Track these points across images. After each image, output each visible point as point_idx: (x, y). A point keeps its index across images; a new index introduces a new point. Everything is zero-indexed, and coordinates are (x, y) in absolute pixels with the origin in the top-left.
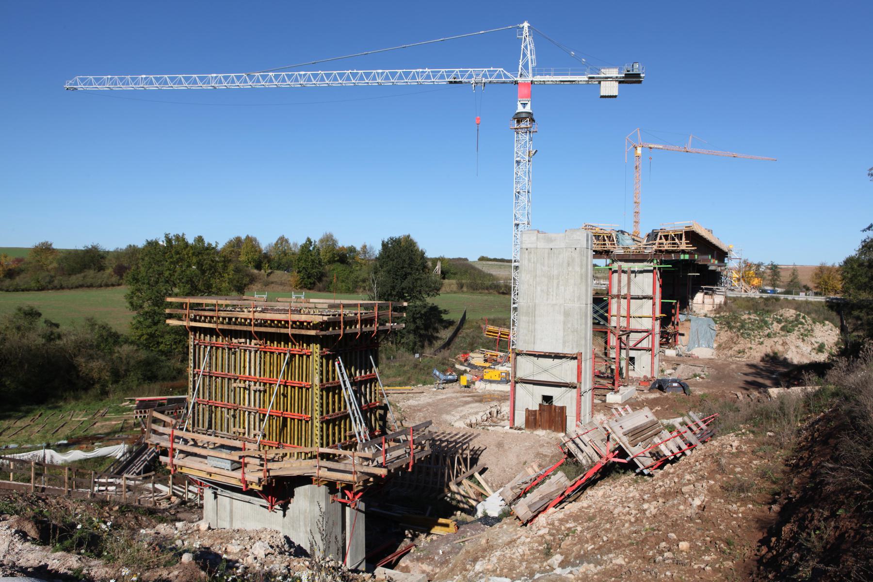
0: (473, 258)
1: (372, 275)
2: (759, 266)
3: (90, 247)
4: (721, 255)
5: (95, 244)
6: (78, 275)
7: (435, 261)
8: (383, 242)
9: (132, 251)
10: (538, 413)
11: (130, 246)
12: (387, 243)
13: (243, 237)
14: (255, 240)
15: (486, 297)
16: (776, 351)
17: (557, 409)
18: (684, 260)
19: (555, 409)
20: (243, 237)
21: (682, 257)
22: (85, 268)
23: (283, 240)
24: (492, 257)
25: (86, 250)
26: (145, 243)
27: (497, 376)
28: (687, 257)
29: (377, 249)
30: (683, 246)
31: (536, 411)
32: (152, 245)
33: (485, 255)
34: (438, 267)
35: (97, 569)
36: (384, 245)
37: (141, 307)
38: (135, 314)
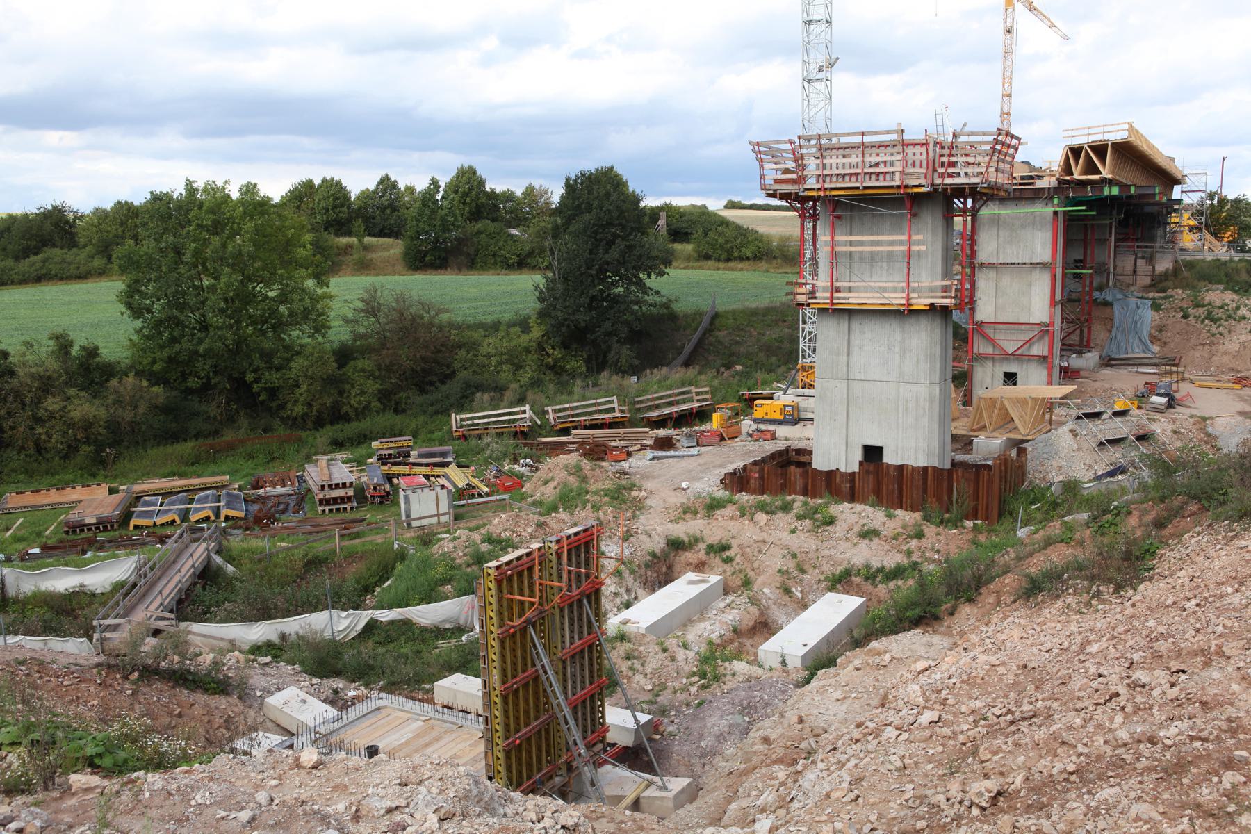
0: (715, 205)
1: (548, 243)
2: (76, 212)
3: (50, 208)
4: (1169, 180)
5: (58, 203)
6: (33, 258)
7: (654, 213)
8: (568, 180)
9: (125, 212)
10: (857, 476)
11: (119, 203)
12: (575, 181)
13: (317, 181)
14: (339, 183)
15: (720, 275)
16: (59, 331)
17: (891, 470)
18: (1113, 198)
19: (912, 474)
20: (317, 181)
21: (1106, 191)
22: (45, 245)
23: (387, 184)
24: (748, 203)
25: (43, 213)
26: (149, 197)
27: (778, 412)
28: (1115, 191)
29: (556, 194)
30: (1106, 173)
31: (853, 474)
32: (160, 201)
33: (736, 200)
34: (662, 222)
35: (1045, 825)
36: (570, 186)
37: (149, 311)
38: (139, 323)
